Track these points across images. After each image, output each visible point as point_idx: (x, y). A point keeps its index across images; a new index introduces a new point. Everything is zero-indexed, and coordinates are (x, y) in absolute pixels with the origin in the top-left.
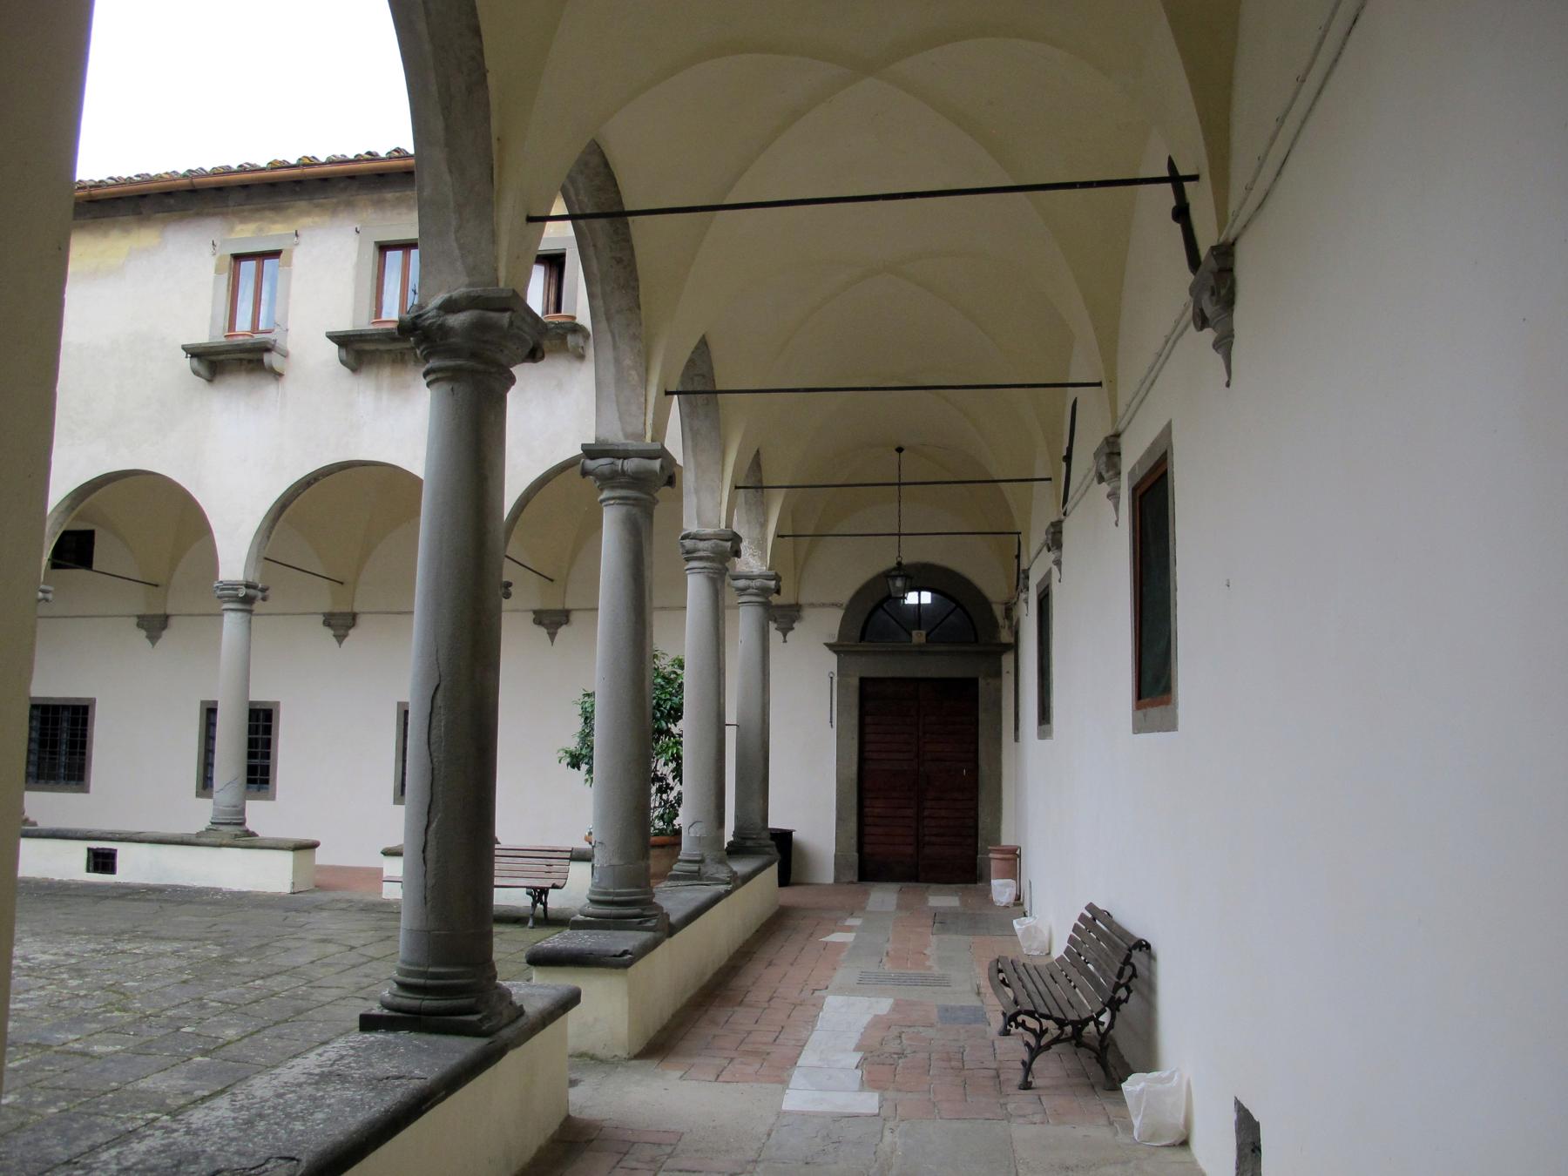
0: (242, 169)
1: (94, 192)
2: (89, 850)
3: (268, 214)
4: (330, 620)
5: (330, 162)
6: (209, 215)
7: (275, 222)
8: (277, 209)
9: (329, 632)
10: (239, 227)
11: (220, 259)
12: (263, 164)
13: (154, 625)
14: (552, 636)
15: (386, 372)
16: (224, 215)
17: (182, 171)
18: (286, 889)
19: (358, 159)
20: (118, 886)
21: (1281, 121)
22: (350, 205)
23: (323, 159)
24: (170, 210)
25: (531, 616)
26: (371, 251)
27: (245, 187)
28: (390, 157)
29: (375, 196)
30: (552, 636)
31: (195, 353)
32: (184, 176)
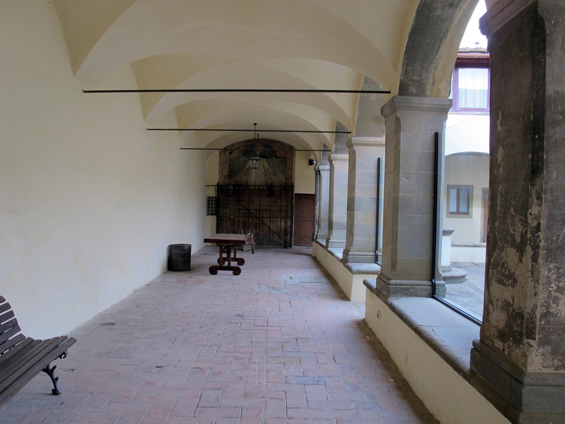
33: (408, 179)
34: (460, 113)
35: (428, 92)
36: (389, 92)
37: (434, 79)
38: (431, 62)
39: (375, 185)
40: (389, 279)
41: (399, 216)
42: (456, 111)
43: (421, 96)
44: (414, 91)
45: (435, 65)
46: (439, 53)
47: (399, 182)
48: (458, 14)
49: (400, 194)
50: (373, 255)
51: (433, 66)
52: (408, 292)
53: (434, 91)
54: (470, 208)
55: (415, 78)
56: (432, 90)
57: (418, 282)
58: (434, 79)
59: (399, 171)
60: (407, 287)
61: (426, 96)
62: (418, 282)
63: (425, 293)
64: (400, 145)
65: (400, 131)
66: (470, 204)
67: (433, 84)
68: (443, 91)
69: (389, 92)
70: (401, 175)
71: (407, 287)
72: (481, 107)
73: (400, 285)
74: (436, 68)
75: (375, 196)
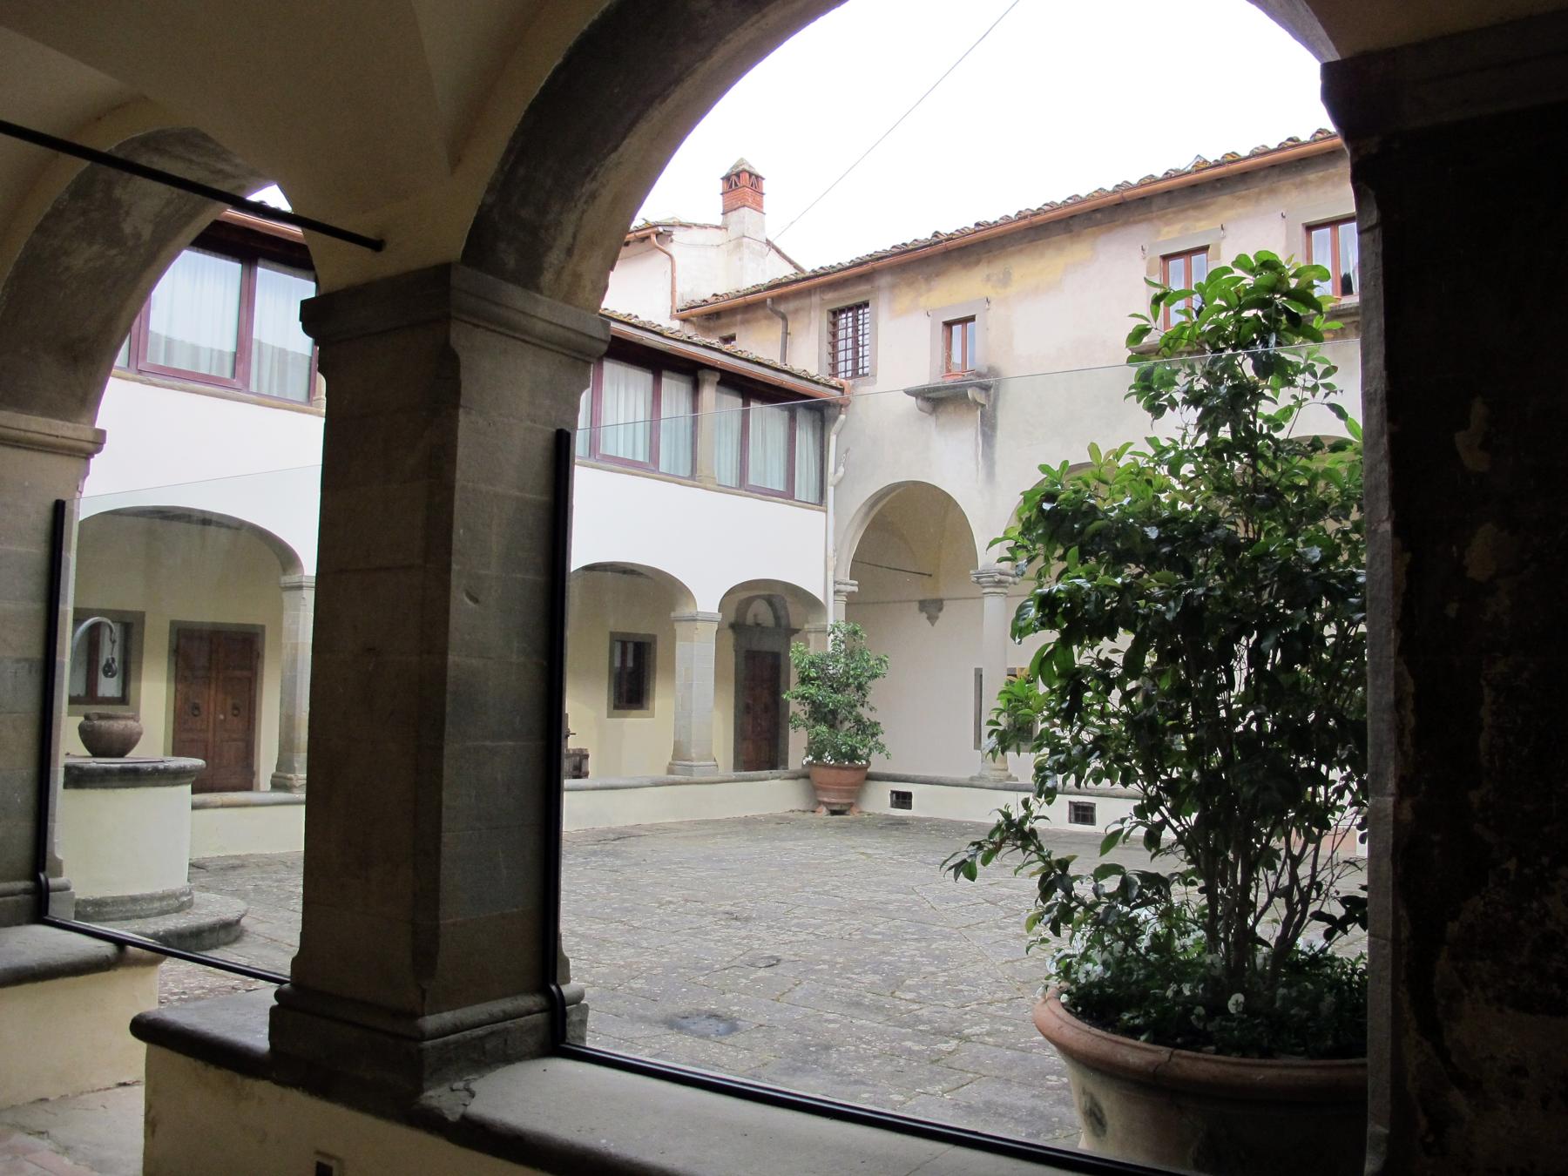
0: (1168, 176)
1: (1035, 219)
2: (66, 786)
3: (1191, 213)
4: (923, 605)
5: (1253, 155)
6: (1135, 222)
7: (1199, 220)
8: (1200, 207)
10: (1165, 230)
11: (1151, 262)
12: (1273, 145)
13: (932, 608)
16: (1149, 220)
17: (1110, 188)
19: (1281, 148)
20: (914, 819)
21: (705, 346)
22: (1272, 191)
23: (1159, 175)
24: (1098, 224)
26: (1301, 231)
27: (1168, 193)
28: (1314, 140)
29: (1298, 180)
31: (919, 393)
32: (1114, 192)
33: (476, 600)
34: (155, 380)
35: (547, 277)
36: (376, 245)
37: (574, 237)
38: (588, 172)
39: (37, 607)
40: (414, 1015)
41: (447, 751)
42: (140, 372)
43: (525, 286)
44: (511, 261)
45: (594, 185)
46: (621, 149)
47: (447, 611)
48: (745, 34)
49: (452, 658)
50: (25, 891)
51: (589, 187)
52: (490, 1052)
53: (566, 277)
54: (133, 685)
55: (526, 213)
56: (559, 273)
57: (507, 1005)
58: (574, 237)
59: (449, 565)
60: (479, 1032)
61: (539, 290)
62: (507, 1005)
63: (531, 1042)
64: (454, 461)
65: (456, 406)
66: (133, 667)
67: (569, 252)
68: (589, 287)
69: (376, 245)
70: (454, 581)
71: (479, 1032)
72: (214, 373)
73: (456, 1029)
74: (593, 196)
75: (36, 652)
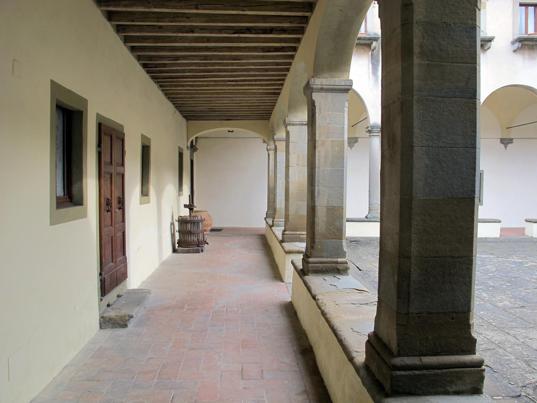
9: (503, 145)
14: (506, 147)
15: (527, 52)
18: (498, 236)
25: (499, 140)
30: (506, 147)
